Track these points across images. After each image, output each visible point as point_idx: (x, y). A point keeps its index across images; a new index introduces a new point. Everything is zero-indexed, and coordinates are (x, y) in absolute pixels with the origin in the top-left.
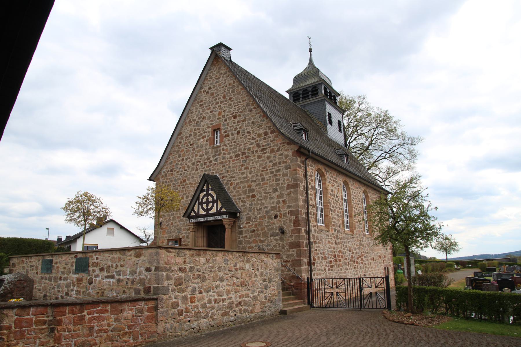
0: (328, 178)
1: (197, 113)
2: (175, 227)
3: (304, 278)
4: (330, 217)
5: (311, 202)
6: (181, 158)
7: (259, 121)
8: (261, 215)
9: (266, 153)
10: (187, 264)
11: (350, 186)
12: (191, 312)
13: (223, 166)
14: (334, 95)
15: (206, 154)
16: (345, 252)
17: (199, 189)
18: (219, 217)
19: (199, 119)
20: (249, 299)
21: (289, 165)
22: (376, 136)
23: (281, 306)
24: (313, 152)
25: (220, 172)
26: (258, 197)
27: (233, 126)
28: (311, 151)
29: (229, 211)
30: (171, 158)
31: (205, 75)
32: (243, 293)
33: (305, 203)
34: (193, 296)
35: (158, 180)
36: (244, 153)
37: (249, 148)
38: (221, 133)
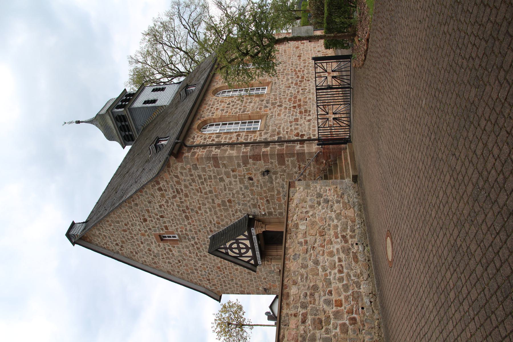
0: (208, 115)
1: (145, 257)
2: (267, 276)
3: (318, 148)
4: (251, 113)
5: (234, 139)
6: (195, 271)
7: (147, 196)
8: (250, 194)
9: (182, 190)
10: (298, 311)
11: (218, 86)
12: (353, 306)
13: (200, 231)
14: (121, 102)
15: (189, 248)
16: (291, 93)
17: (225, 256)
18: (254, 237)
19: (151, 255)
20: (339, 224)
21: (193, 165)
22: (172, 44)
23: (348, 181)
24: (178, 138)
25: (206, 234)
26: (230, 197)
27: (156, 222)
28: (177, 141)
29: (246, 228)
30: (195, 281)
31: (103, 250)
32: (332, 232)
33: (234, 147)
34: (334, 302)
35: (220, 293)
36: (184, 211)
37: (177, 206)
38: (164, 234)
